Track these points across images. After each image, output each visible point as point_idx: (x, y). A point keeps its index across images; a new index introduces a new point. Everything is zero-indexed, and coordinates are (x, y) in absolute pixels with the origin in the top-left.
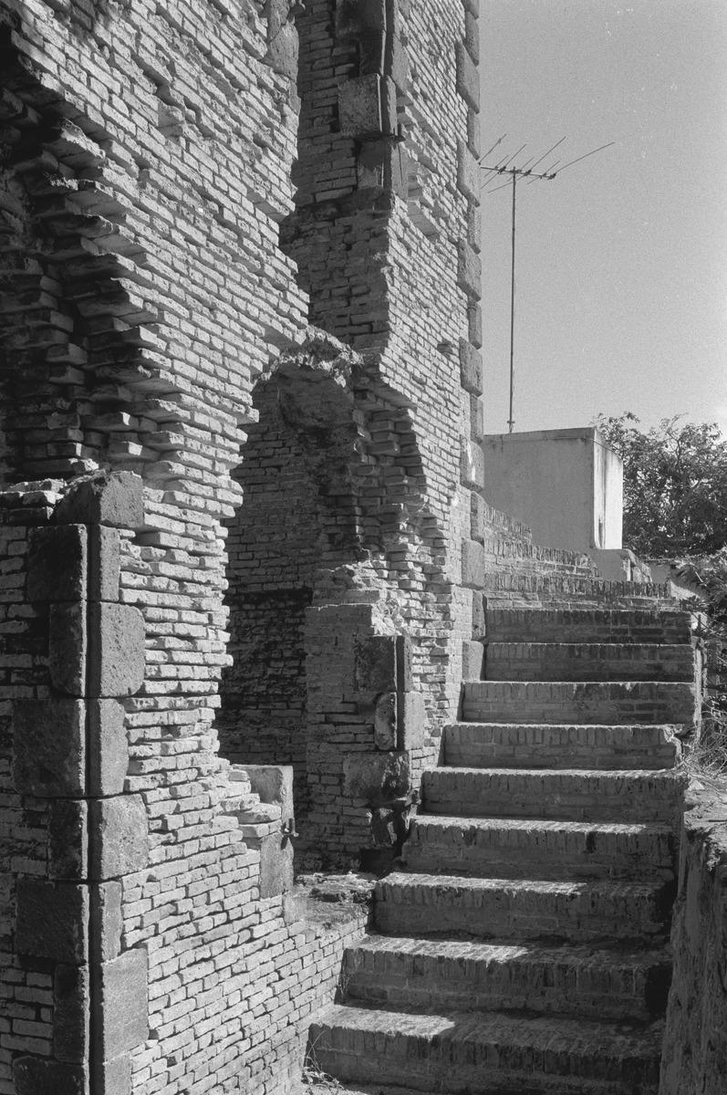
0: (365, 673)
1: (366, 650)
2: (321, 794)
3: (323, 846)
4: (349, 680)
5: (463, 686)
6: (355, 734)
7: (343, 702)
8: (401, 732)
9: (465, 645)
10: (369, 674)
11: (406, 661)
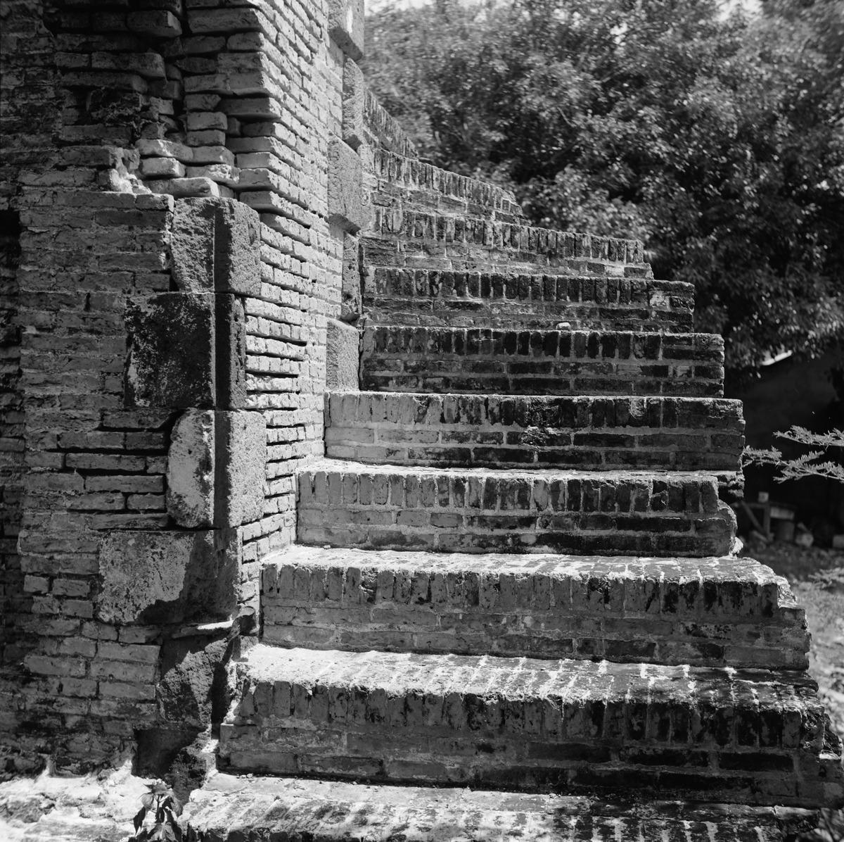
0: (149, 370)
1: (150, 322)
2: (51, 616)
3: (57, 722)
4: (114, 384)
5: (328, 401)
6: (126, 495)
7: (101, 428)
8: (223, 487)
9: (331, 327)
10: (156, 372)
11: (233, 346)
